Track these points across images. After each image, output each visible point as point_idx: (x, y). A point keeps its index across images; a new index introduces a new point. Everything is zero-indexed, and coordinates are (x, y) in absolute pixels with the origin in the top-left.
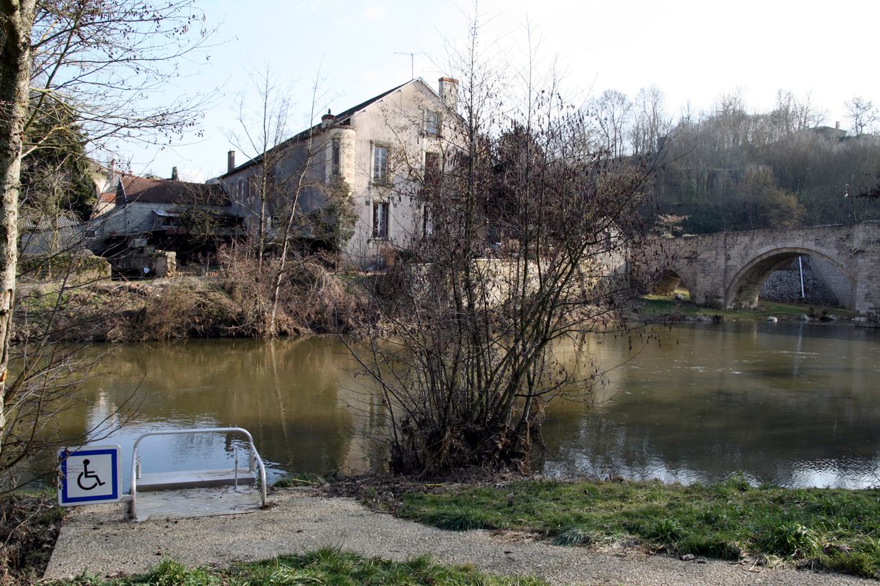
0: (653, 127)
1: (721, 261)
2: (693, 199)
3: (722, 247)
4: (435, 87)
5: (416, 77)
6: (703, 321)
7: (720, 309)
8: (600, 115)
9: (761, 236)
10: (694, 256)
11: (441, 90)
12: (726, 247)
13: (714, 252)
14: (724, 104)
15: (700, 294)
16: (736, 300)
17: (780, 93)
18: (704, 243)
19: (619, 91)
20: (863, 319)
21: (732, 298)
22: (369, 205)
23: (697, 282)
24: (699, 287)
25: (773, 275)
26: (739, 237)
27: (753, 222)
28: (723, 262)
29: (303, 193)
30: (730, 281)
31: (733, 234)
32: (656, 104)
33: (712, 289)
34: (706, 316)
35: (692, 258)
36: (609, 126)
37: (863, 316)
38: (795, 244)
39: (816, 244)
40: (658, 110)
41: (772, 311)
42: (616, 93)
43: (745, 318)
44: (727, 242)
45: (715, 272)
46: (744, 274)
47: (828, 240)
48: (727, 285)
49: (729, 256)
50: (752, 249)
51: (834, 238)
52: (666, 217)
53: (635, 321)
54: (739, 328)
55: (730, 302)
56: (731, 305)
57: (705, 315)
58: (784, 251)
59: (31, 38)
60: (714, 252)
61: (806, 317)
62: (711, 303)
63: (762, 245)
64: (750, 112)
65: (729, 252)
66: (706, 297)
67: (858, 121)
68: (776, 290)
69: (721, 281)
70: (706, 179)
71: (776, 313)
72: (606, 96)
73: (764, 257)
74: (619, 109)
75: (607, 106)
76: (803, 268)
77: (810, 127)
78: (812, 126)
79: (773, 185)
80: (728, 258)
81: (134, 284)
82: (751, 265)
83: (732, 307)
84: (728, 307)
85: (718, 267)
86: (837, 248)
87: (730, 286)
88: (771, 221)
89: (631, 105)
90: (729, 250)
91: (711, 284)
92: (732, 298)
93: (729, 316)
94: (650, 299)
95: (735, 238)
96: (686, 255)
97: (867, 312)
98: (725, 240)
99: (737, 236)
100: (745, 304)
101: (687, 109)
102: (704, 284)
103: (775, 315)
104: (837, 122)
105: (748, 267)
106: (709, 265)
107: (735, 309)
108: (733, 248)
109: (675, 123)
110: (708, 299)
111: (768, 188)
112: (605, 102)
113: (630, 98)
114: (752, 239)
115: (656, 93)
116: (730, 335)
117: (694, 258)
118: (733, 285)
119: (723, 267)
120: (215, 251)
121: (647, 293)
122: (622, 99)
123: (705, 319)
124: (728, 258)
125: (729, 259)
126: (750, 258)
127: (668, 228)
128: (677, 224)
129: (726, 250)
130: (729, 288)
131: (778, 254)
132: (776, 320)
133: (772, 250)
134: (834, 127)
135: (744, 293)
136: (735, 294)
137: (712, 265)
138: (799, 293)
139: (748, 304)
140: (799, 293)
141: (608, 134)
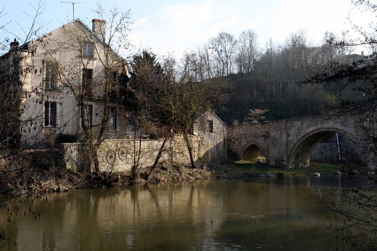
0: (251, 56)
1: (284, 138)
2: (274, 99)
3: (284, 129)
4: (90, 27)
5: (75, 18)
6: (271, 177)
7: (285, 169)
8: (217, 48)
9: (308, 121)
10: (267, 135)
11: (94, 27)
12: (287, 128)
13: (280, 132)
14: (293, 41)
15: (272, 159)
16: (294, 163)
17: (326, 34)
18: (273, 126)
19: (228, 33)
20: (373, 173)
21: (292, 161)
22: (42, 103)
23: (270, 151)
24: (271, 155)
25: (319, 145)
26: (294, 122)
27: (311, 113)
28: (285, 138)
30: (290, 151)
31: (291, 120)
32: (251, 41)
33: (279, 156)
34: (272, 173)
35: (266, 136)
36: (223, 55)
38: (329, 125)
39: (342, 125)
40: (254, 45)
41: (319, 169)
42: (227, 34)
43: (300, 174)
44: (287, 125)
45: (281, 145)
46: (299, 146)
47: (349, 122)
48: (289, 153)
49: (289, 134)
50: (303, 129)
51: (352, 121)
52: (254, 110)
53: (225, 178)
54: (297, 181)
55: (291, 163)
56: (292, 166)
57: (272, 173)
58: (322, 130)
59: (58, 53)
60: (280, 132)
61: (339, 172)
62: (279, 165)
63: (308, 126)
64: (308, 44)
65: (288, 132)
66: (276, 161)
67: (374, 51)
68: (323, 155)
69: (285, 150)
70: (281, 86)
71: (320, 170)
72: (221, 36)
73: (311, 134)
74: (229, 44)
75: (222, 42)
76: (339, 141)
77: (346, 54)
78: (347, 54)
79: (322, 89)
80: (288, 136)
82: (303, 140)
83: (292, 167)
84: (290, 167)
85: (282, 142)
86: (354, 127)
87: (290, 154)
88: (321, 112)
89: (236, 41)
90: (289, 130)
91: (279, 152)
92: (292, 161)
93: (289, 173)
94: (241, 163)
95: (292, 123)
96: (263, 134)
97: (375, 168)
98: (286, 124)
99: (293, 121)
100: (301, 165)
101: (270, 44)
102: (274, 152)
103: (319, 172)
104: (362, 51)
105: (301, 141)
106: (277, 140)
107: (295, 168)
108: (291, 129)
109: (264, 52)
110: (277, 162)
111: (319, 91)
112: (221, 40)
113: (236, 37)
114: (302, 123)
115: (251, 35)
116: (292, 187)
117: (268, 136)
118: (292, 153)
119: (285, 141)
120: (81, 187)
121: (239, 159)
122: (230, 38)
123: (272, 175)
124: (288, 136)
125: (289, 136)
126: (302, 135)
127: (256, 117)
128: (262, 115)
129: (287, 130)
130: (289, 155)
131: (318, 132)
132: (319, 175)
133: (315, 130)
134: (361, 54)
135: (300, 158)
136: (294, 159)
137: (279, 140)
138: (337, 157)
139: (303, 164)
140: (337, 157)
141: (223, 60)
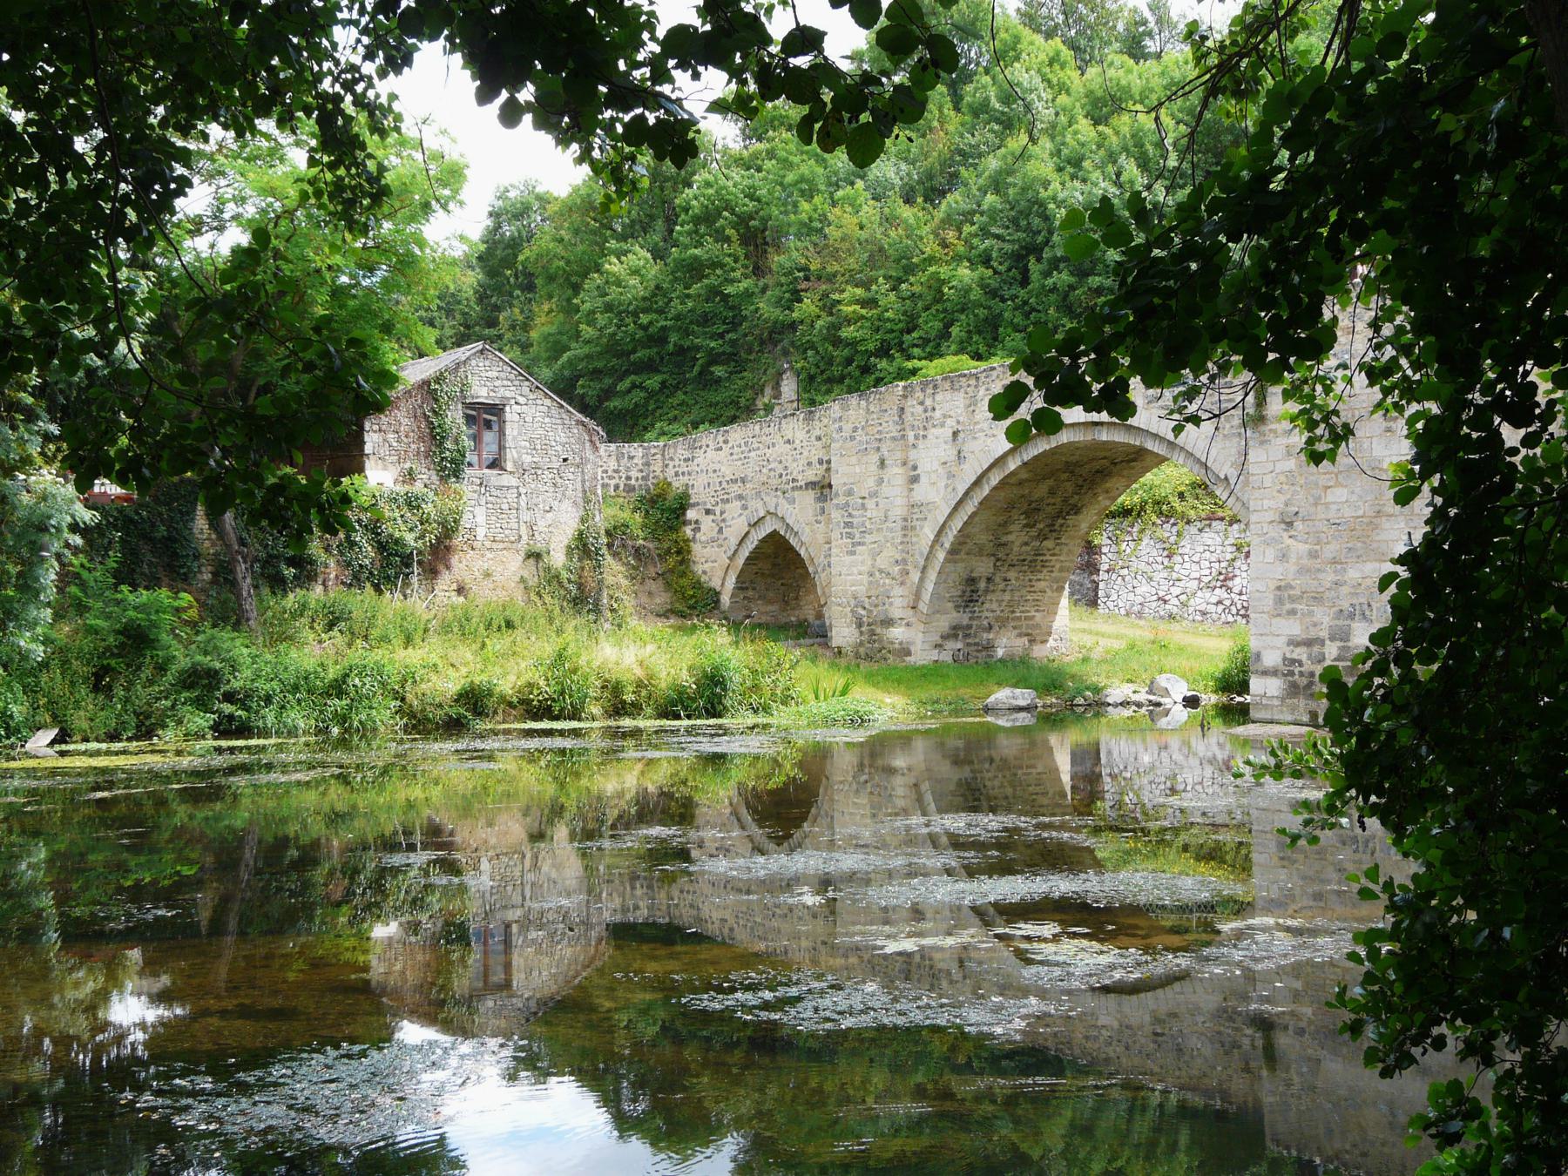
26: (939, 397)
29: (1047, 1100)
37: (1274, 673)
49: (915, 468)
81: (34, 784)
95: (928, 402)
105: (970, 507)
108: (925, 437)
119: (898, 511)
135: (991, 607)
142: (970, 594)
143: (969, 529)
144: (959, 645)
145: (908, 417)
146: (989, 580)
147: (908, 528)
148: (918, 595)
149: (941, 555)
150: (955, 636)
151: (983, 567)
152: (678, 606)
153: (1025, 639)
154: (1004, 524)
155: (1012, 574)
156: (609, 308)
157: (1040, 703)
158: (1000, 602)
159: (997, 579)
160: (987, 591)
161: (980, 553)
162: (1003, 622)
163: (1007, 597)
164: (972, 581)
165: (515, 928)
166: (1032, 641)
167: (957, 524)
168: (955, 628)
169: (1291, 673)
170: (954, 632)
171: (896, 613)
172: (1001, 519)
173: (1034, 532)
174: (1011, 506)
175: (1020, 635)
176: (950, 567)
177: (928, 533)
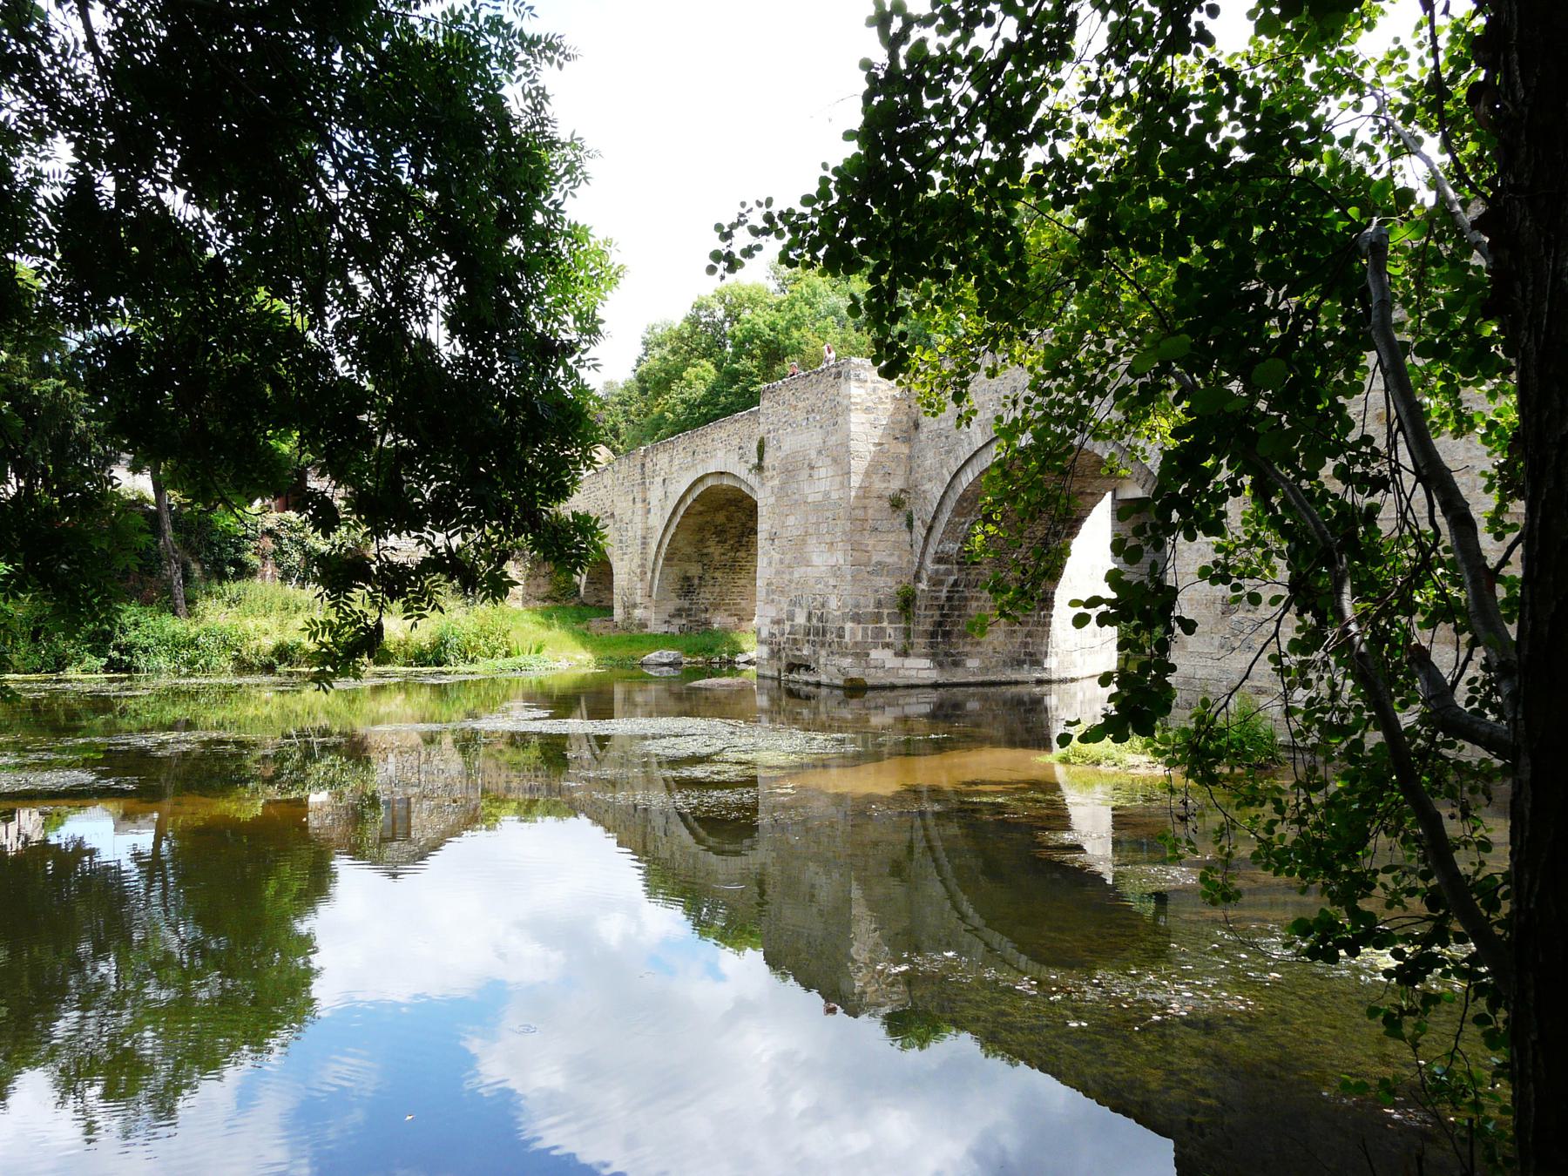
105: (672, 530)
135: (706, 596)
142: (687, 587)
143: (675, 545)
144: (684, 622)
145: (646, 470)
146: (700, 578)
147: (645, 544)
148: (651, 587)
149: (661, 561)
150: (681, 616)
151: (694, 570)
152: (554, 595)
153: (735, 619)
154: (701, 541)
155: (718, 574)
156: (683, 401)
157: (685, 660)
158: (712, 593)
159: (707, 577)
160: (700, 586)
161: (689, 559)
162: (716, 607)
163: (717, 589)
164: (687, 579)
165: (413, 800)
166: (741, 620)
167: (667, 541)
168: (679, 610)
169: (771, 643)
170: (679, 613)
171: (638, 600)
172: (697, 538)
173: (727, 546)
174: (701, 529)
175: (730, 615)
176: (668, 570)
177: (654, 547)
